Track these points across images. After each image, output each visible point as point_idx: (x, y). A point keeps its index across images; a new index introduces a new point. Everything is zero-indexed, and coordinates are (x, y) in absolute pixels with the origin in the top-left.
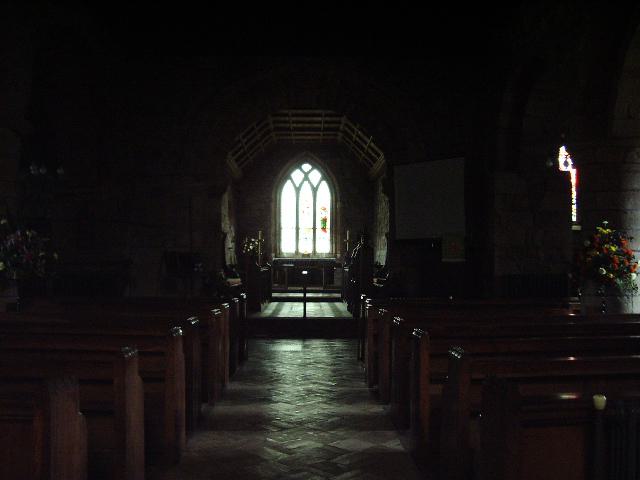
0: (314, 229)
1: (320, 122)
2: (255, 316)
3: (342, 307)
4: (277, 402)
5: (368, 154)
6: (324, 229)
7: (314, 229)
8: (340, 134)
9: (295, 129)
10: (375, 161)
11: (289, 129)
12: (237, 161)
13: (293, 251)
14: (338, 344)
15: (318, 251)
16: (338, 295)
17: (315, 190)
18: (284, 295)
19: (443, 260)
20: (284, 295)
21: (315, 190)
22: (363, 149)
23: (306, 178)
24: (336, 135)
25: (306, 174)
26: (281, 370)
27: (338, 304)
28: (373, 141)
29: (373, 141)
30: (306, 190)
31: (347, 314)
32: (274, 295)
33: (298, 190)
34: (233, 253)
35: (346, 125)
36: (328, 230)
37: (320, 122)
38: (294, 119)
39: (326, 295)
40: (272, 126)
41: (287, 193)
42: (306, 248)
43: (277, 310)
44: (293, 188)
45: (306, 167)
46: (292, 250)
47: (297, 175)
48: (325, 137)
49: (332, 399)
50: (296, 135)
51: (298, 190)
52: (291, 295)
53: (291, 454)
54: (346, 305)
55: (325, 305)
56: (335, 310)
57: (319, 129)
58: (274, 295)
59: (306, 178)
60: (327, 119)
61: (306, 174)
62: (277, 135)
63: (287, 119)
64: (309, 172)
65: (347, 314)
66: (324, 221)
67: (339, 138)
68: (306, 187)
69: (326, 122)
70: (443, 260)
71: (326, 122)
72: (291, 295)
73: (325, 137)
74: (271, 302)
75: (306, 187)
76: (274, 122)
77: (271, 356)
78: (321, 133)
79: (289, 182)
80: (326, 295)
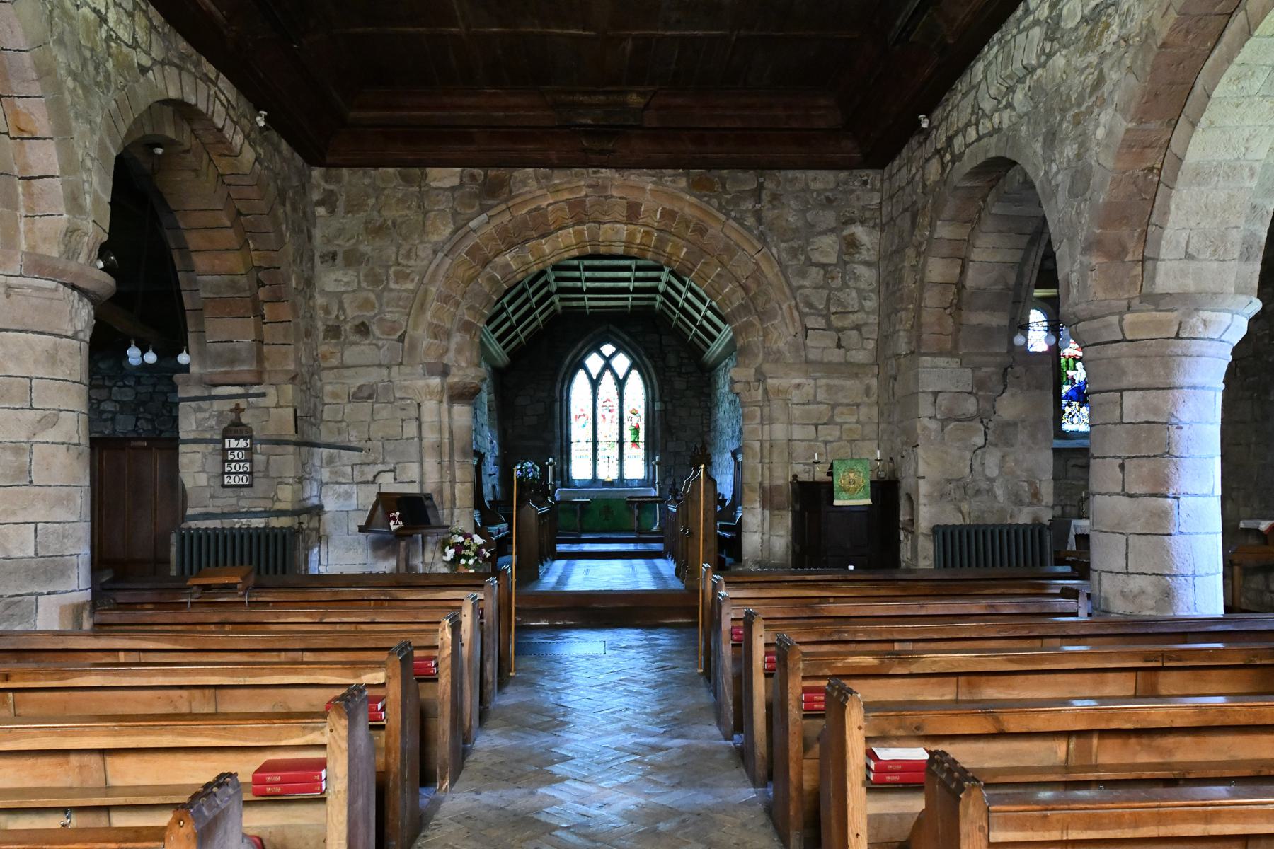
0: (621, 442)
1: (628, 280)
2: (531, 589)
3: (666, 567)
4: (562, 780)
5: (701, 328)
6: (635, 443)
7: (621, 442)
8: (659, 298)
9: (590, 291)
10: (713, 338)
11: (579, 290)
12: (500, 339)
13: (589, 476)
14: (663, 639)
15: (627, 476)
16: (657, 547)
17: (621, 383)
18: (576, 548)
19: (836, 503)
20: (576, 548)
21: (621, 383)
22: (694, 320)
23: (607, 366)
24: (654, 299)
25: (608, 360)
26: (570, 699)
27: (659, 563)
28: (585, 307)
29: (585, 307)
30: (608, 386)
31: (676, 585)
32: (561, 547)
33: (595, 384)
34: (496, 482)
35: (669, 284)
36: (642, 446)
37: (628, 280)
38: (588, 274)
39: (641, 547)
40: (554, 286)
41: (580, 387)
42: (608, 472)
43: (563, 579)
44: (587, 381)
45: (608, 349)
46: (588, 475)
47: (594, 363)
48: (635, 303)
49: (658, 768)
50: (590, 299)
51: (595, 384)
52: (587, 547)
53: (594, 841)
54: (674, 566)
55: (639, 564)
56: (657, 575)
57: (626, 290)
58: (561, 547)
59: (607, 366)
60: (640, 274)
61: (608, 360)
62: (561, 300)
63: (577, 274)
64: (613, 355)
65: (676, 585)
66: (636, 430)
67: (558, 305)
68: (608, 383)
69: (637, 280)
70: (836, 503)
71: (637, 280)
72: (587, 547)
73: (635, 303)
74: (553, 560)
75: (608, 383)
76: (558, 279)
77: (554, 668)
78: (630, 297)
79: (581, 373)
80: (641, 547)
